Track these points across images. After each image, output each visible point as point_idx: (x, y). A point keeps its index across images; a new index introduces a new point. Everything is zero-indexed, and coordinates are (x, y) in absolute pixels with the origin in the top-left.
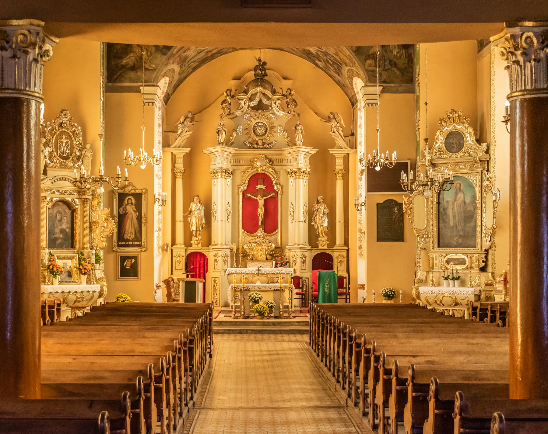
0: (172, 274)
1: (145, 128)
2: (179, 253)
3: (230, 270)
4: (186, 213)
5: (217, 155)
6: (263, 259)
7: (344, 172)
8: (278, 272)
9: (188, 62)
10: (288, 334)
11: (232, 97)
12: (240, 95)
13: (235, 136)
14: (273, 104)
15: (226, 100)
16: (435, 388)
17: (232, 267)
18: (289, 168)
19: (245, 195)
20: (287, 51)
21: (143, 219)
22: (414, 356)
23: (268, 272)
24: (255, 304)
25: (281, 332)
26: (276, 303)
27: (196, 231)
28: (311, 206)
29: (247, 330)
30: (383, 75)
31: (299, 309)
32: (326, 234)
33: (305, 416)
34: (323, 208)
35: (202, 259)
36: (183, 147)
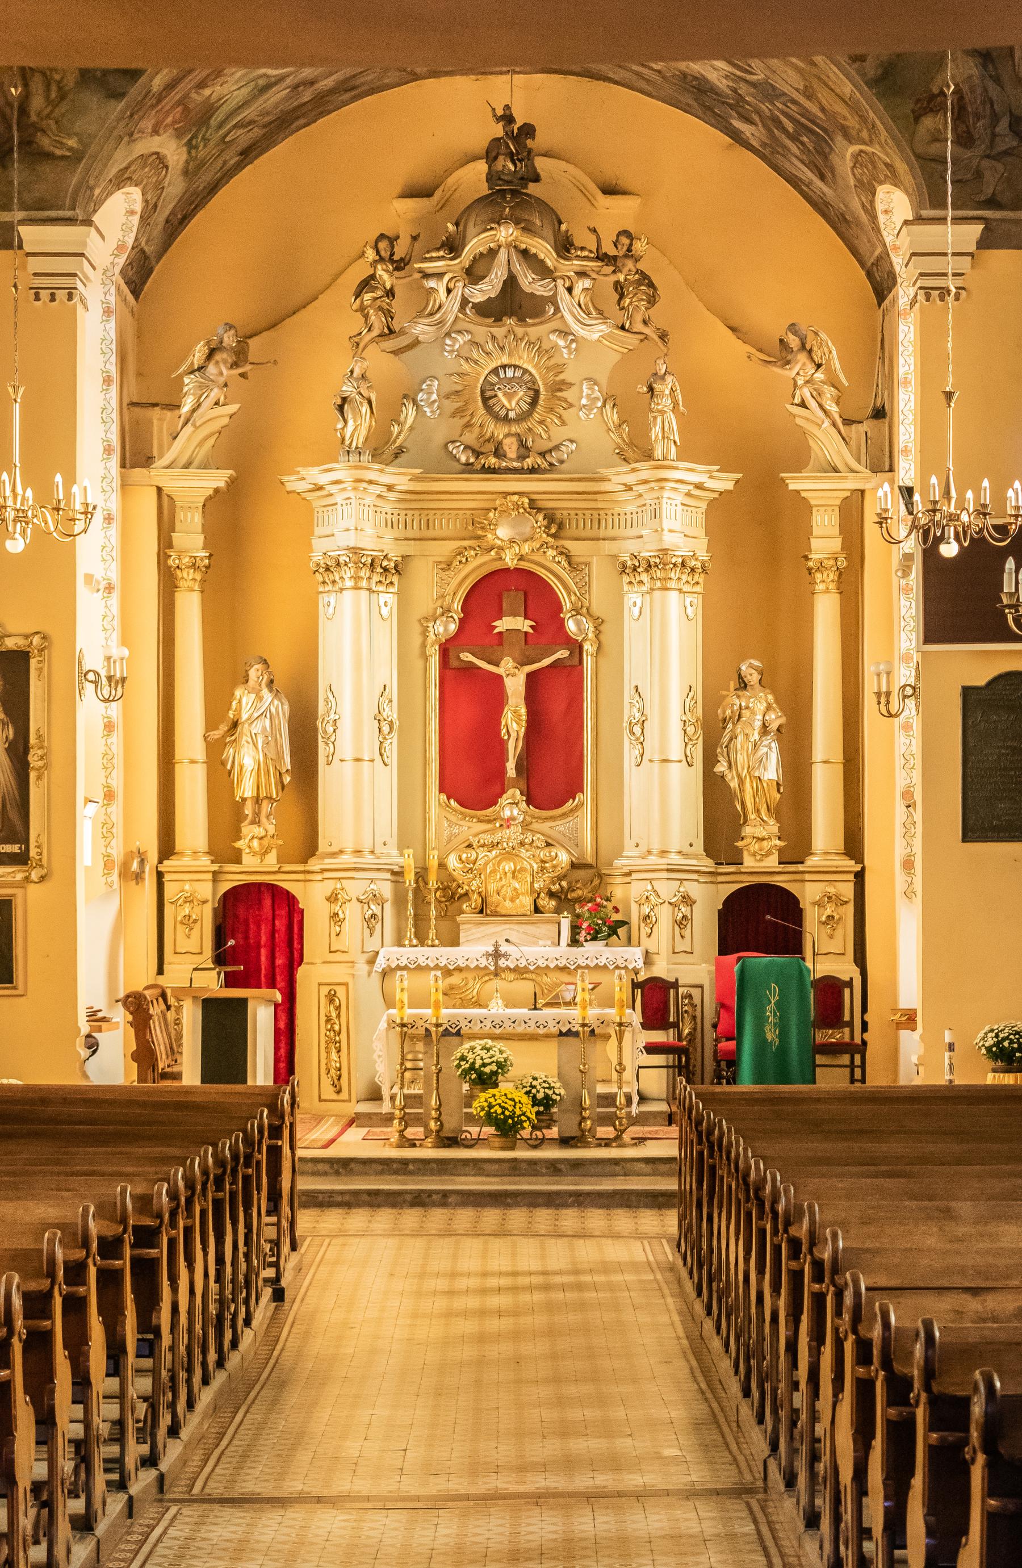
0: (160, 971)
1: (22, 390)
2: (187, 887)
3: (390, 954)
4: (217, 728)
5: (339, 499)
6: (521, 911)
7: (842, 563)
8: (582, 962)
9: (220, 125)
10: (608, 1207)
11: (400, 265)
12: (432, 259)
13: (410, 421)
14: (562, 292)
15: (372, 277)
16: (986, 1414)
17: (400, 944)
18: (626, 549)
19: (452, 655)
20: (616, 83)
21: (32, 752)
22: (975, 1291)
23: (541, 963)
24: (484, 1090)
25: (580, 1200)
26: (565, 1086)
27: (257, 801)
28: (712, 700)
29: (445, 1194)
30: (987, 174)
31: (663, 1107)
32: (776, 812)
33: (589, 1527)
34: (761, 707)
35: (283, 912)
36: (204, 466)
